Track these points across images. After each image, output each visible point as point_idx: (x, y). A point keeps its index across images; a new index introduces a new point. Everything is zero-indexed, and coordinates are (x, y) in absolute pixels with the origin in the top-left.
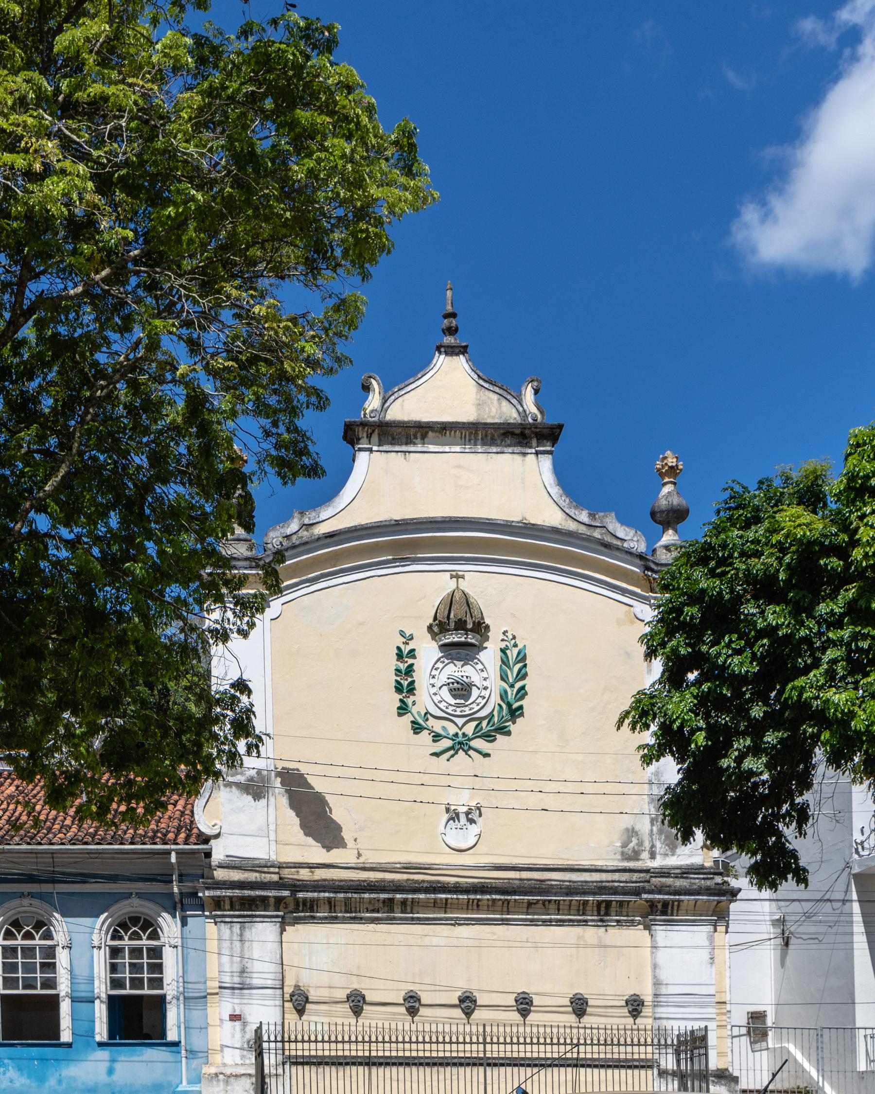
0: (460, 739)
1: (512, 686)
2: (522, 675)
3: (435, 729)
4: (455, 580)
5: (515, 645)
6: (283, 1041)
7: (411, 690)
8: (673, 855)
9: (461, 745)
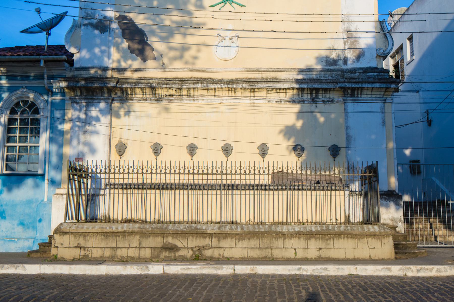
6: (143, 174)
8: (358, 62)
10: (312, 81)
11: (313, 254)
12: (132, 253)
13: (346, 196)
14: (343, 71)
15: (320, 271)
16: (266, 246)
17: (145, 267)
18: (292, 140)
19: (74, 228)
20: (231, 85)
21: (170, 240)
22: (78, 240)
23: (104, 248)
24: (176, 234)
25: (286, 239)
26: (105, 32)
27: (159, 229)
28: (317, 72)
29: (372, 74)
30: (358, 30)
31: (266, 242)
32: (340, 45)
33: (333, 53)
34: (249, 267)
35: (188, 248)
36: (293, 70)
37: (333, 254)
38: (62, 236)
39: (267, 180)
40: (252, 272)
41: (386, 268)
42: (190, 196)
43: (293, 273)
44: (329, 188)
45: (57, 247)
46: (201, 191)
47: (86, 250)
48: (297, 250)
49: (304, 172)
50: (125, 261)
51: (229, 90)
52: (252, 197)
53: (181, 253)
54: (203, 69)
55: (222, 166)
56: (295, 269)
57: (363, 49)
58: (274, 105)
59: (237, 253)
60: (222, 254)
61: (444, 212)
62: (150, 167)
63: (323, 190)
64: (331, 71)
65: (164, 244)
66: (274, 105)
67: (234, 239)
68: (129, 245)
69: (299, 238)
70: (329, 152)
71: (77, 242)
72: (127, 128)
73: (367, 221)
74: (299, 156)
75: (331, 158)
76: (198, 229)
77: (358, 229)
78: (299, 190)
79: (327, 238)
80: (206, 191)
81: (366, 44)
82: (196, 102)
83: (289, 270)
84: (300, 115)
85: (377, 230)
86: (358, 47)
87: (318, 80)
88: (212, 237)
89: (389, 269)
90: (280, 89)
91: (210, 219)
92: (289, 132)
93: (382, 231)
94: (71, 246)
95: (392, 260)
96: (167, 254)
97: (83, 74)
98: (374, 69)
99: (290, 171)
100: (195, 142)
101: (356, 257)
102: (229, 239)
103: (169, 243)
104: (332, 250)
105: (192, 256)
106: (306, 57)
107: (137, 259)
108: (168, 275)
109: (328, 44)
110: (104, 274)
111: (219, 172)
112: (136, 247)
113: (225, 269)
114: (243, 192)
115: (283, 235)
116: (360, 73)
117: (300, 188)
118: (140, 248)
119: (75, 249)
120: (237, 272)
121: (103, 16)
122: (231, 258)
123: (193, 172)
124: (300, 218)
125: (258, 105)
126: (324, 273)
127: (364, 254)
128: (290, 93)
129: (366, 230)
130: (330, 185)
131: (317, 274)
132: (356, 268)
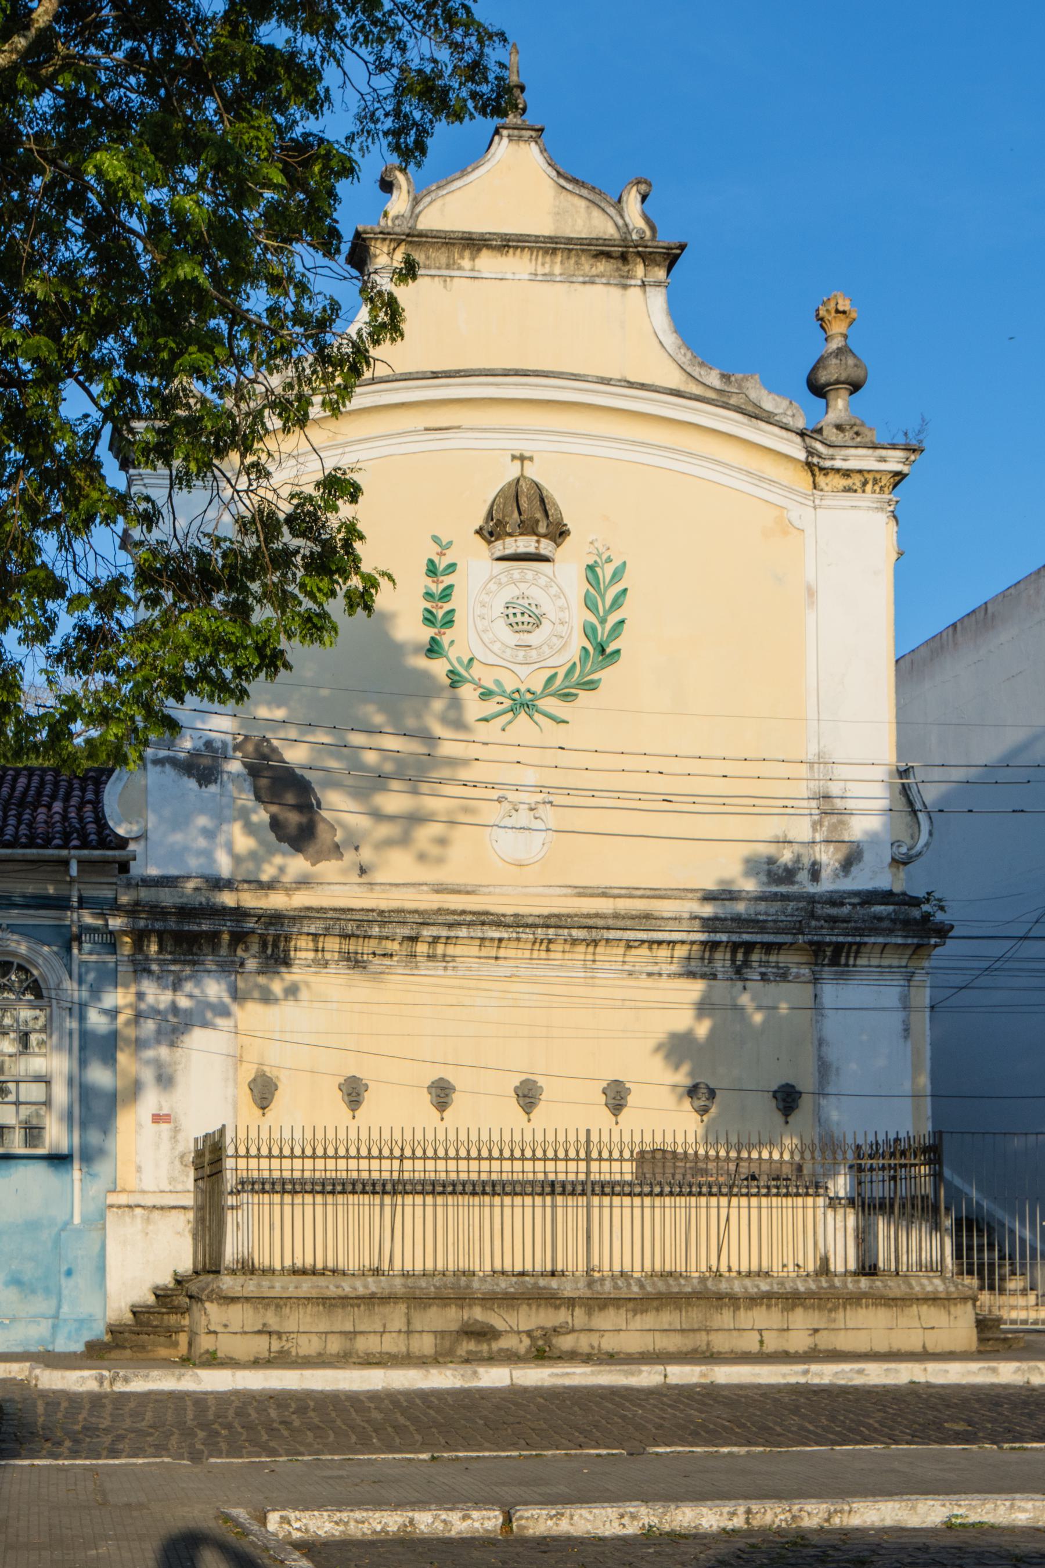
1: (603, 621)
2: (617, 603)
3: (483, 683)
8: (845, 876)
10: (740, 922)
11: (799, 1342)
12: (391, 1344)
13: (820, 1212)
14: (812, 900)
15: (850, 1375)
16: (696, 1327)
17: (470, 1372)
18: (685, 1068)
19: (252, 1288)
20: (549, 930)
21: (478, 1314)
22: (264, 1316)
23: (326, 1333)
24: (490, 1300)
25: (739, 1308)
26: (210, 782)
27: (452, 1290)
28: (749, 900)
29: (883, 907)
30: (848, 794)
31: (694, 1316)
32: (801, 830)
33: (785, 852)
34: (697, 1369)
35: (519, 1332)
36: (690, 895)
37: (843, 1342)
38: (224, 1308)
39: (627, 1171)
40: (703, 1381)
41: (989, 1368)
42: (440, 1210)
43: (793, 1380)
44: (811, 1191)
45: (215, 1333)
46: (477, 1199)
47: (284, 1338)
48: (764, 1333)
49: (722, 1153)
50: (370, 1361)
51: (534, 942)
52: (754, 1212)
53: (504, 1343)
54: (469, 889)
55: (588, 1141)
56: (796, 1373)
57: (858, 843)
58: (641, 984)
59: (632, 1342)
60: (596, 1345)
61: (970, 1248)
63: (680, 1194)
64: (785, 898)
65: (465, 1324)
66: (641, 984)
67: (623, 1311)
68: (384, 1326)
69: (769, 1307)
70: (774, 1103)
71: (261, 1322)
72: (277, 1036)
73: (868, 1268)
74: (703, 1111)
75: (779, 1118)
76: (539, 1288)
77: (899, 1286)
78: (711, 1194)
79: (830, 1305)
80: (487, 1199)
81: (866, 833)
82: (450, 972)
83: (784, 1375)
84: (703, 1008)
85: (941, 1288)
86: (847, 839)
87: (753, 921)
88: (574, 1306)
89: (994, 1370)
90: (660, 943)
91: (498, 1267)
92: (677, 1048)
93: (952, 1289)
94: (246, 1329)
95: (972, 1353)
96: (471, 1346)
97: (167, 898)
98: (886, 897)
99: (680, 1150)
100: (450, 1075)
101: (895, 1348)
102: (611, 1312)
103: (477, 1321)
104: (842, 1332)
105: (528, 1351)
106: (708, 859)
107: (403, 1358)
108: (525, 1390)
109: (771, 827)
110: (380, 1388)
112: (400, 1332)
113: (645, 1374)
114: (518, 1200)
115: (732, 1301)
116: (854, 905)
117: (715, 1190)
118: (409, 1332)
119: (257, 1337)
120: (673, 1380)
121: (203, 740)
122: (618, 1353)
124: (714, 1263)
125: (604, 982)
126: (858, 1381)
127: (913, 1342)
128: (681, 951)
129: (917, 1289)
130: (782, 1183)
131: (842, 1382)
132: (925, 1370)
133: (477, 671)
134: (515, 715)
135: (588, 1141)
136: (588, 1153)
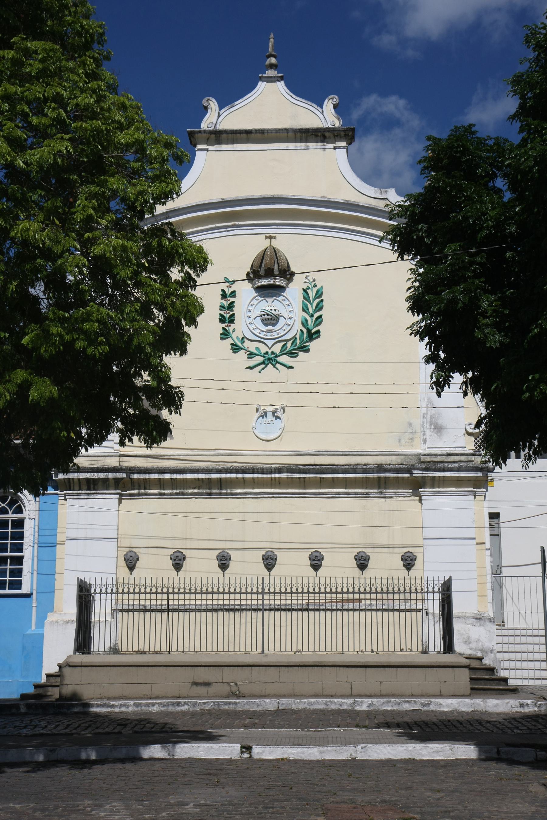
0: (270, 356)
1: (312, 316)
2: (319, 307)
3: (249, 349)
4: (269, 240)
5: (315, 286)
7: (232, 320)
9: (270, 360)
55: (117, 582)
62: (177, 585)
111: (114, 591)
123: (229, 591)
133: (247, 344)
134: (266, 366)
135: (117, 582)
136: (263, 589)
